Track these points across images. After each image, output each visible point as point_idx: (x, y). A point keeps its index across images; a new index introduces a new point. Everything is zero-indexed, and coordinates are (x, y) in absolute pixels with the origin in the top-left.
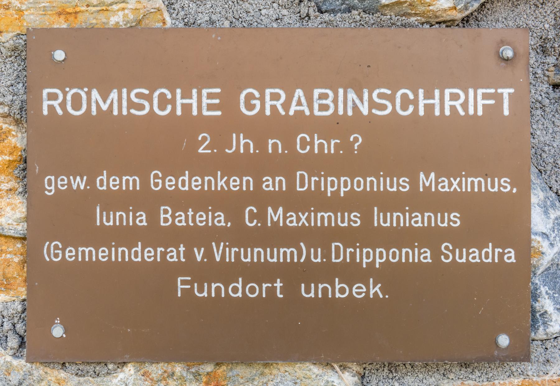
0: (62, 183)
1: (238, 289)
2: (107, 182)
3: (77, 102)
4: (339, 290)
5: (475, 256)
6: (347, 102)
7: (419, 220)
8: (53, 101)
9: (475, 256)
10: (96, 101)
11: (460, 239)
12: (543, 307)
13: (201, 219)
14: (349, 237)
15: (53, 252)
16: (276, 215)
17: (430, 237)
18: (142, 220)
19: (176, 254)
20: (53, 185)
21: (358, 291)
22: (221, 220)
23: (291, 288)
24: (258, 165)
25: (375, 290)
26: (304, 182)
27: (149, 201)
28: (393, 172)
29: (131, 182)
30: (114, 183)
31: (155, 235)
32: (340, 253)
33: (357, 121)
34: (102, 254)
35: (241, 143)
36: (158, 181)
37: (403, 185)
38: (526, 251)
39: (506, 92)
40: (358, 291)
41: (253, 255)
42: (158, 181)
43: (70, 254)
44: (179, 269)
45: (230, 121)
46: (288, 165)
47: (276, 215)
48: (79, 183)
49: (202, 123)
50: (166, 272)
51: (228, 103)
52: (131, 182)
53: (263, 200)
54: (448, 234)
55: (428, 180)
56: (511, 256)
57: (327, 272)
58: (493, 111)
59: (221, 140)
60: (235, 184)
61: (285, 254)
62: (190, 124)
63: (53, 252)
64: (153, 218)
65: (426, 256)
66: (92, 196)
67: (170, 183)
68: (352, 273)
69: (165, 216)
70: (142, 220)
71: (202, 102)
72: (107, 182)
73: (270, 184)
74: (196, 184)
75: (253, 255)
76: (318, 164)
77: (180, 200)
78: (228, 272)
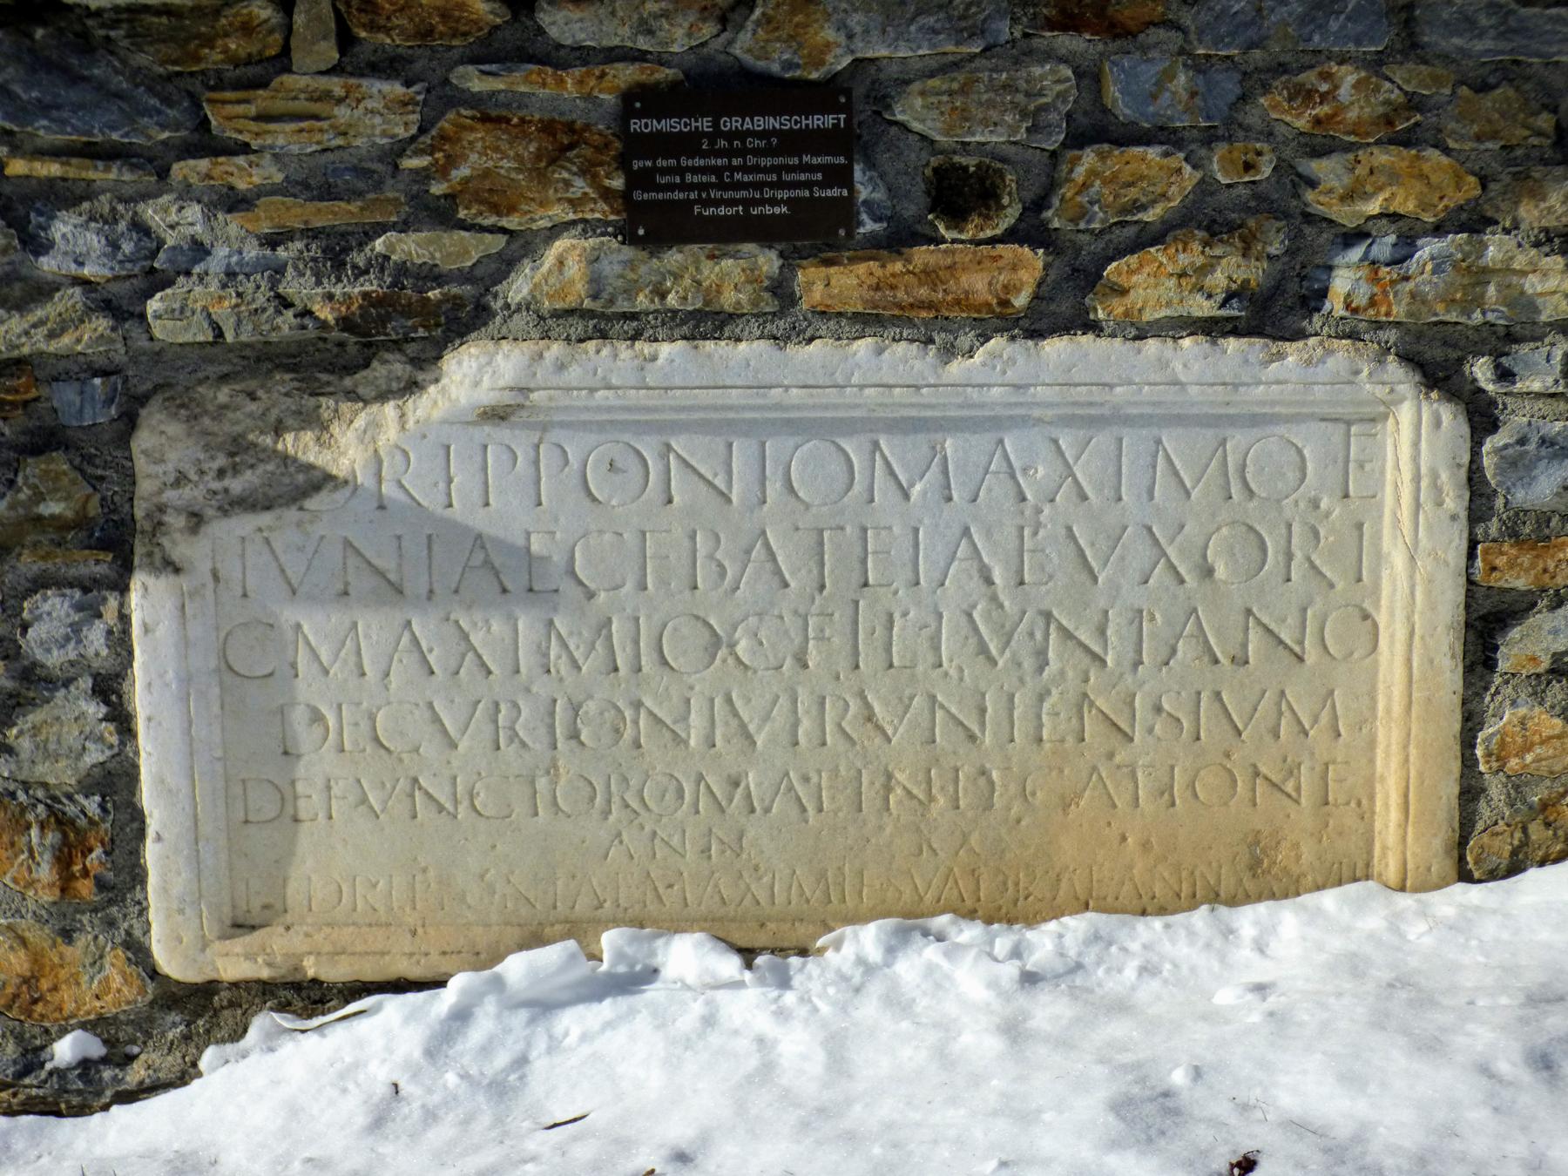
0: (641, 164)
1: (722, 211)
2: (661, 163)
3: (646, 126)
4: (768, 210)
5: (829, 193)
6: (772, 123)
7: (803, 177)
8: (636, 125)
9: (829, 193)
10: (656, 125)
11: (823, 185)
12: (1527, 365)
13: (704, 179)
14: (772, 185)
15: (638, 195)
16: (738, 176)
17: (808, 185)
18: (678, 180)
19: (693, 196)
20: (637, 165)
21: (777, 210)
22: (713, 179)
23: (746, 210)
24: (729, 153)
25: (784, 209)
26: (751, 160)
27: (681, 171)
28: (791, 155)
29: (673, 162)
30: (665, 163)
31: (684, 187)
32: (768, 193)
33: (774, 132)
34: (660, 196)
35: (722, 143)
36: (684, 162)
37: (796, 161)
38: (851, 189)
39: (842, 116)
40: (777, 210)
41: (728, 195)
42: (684, 162)
43: (645, 196)
44: (696, 202)
45: (717, 133)
46: (743, 153)
47: (738, 176)
48: (649, 163)
49: (705, 134)
50: (689, 204)
51: (716, 124)
52: (673, 162)
53: (732, 169)
54: (817, 183)
55: (806, 159)
56: (845, 193)
57: (762, 202)
58: (836, 126)
59: (712, 143)
60: (719, 162)
61: (743, 194)
62: (697, 135)
63: (638, 195)
64: (683, 179)
65: (807, 193)
66: (655, 169)
67: (690, 163)
68: (774, 202)
69: (689, 178)
70: (678, 180)
71: (705, 124)
72: (661, 163)
73: (735, 162)
74: (702, 162)
75: (728, 195)
76: (757, 152)
77: (695, 170)
78: (717, 203)
